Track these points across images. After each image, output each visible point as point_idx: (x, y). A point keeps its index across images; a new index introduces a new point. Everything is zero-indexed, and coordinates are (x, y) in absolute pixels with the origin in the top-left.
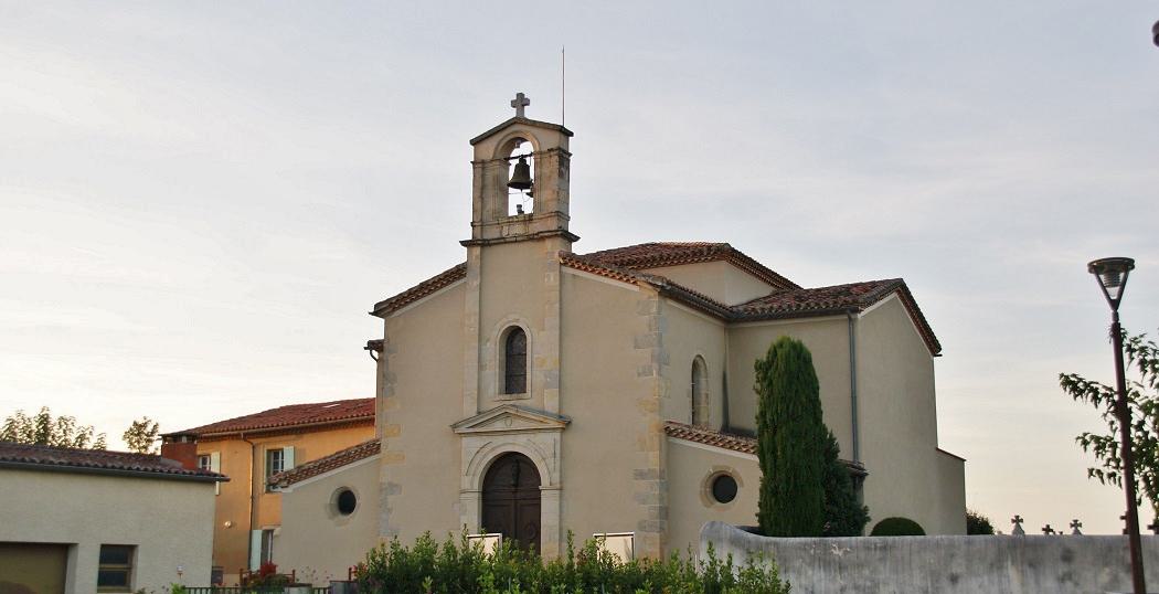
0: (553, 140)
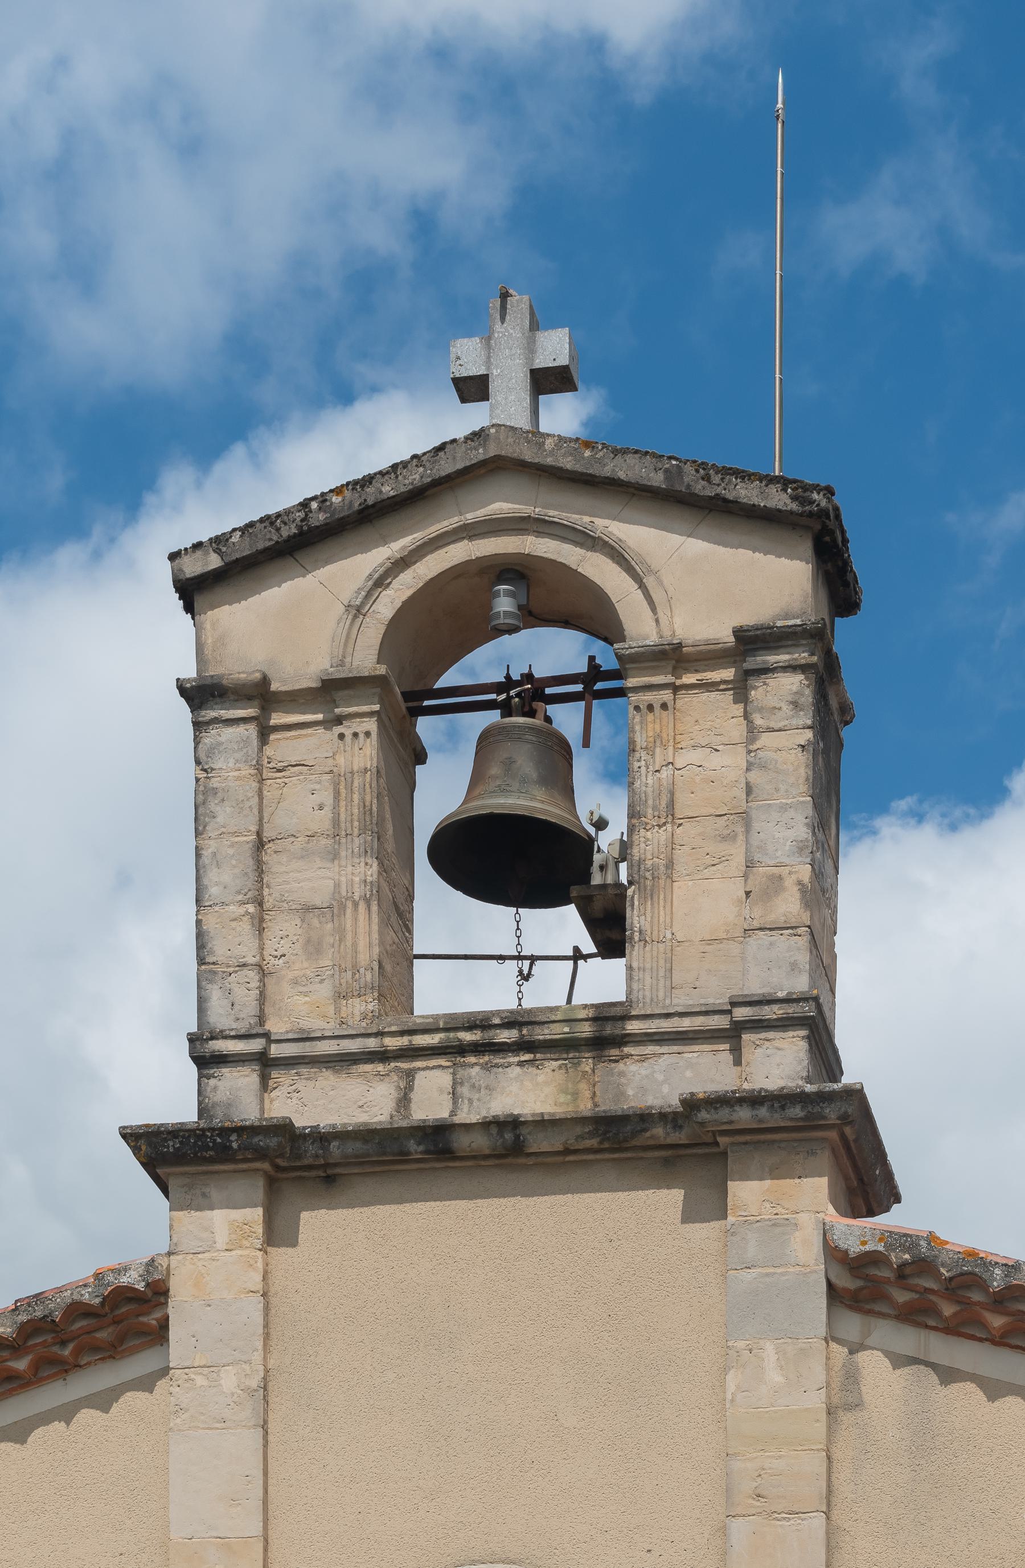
0: (777, 582)
